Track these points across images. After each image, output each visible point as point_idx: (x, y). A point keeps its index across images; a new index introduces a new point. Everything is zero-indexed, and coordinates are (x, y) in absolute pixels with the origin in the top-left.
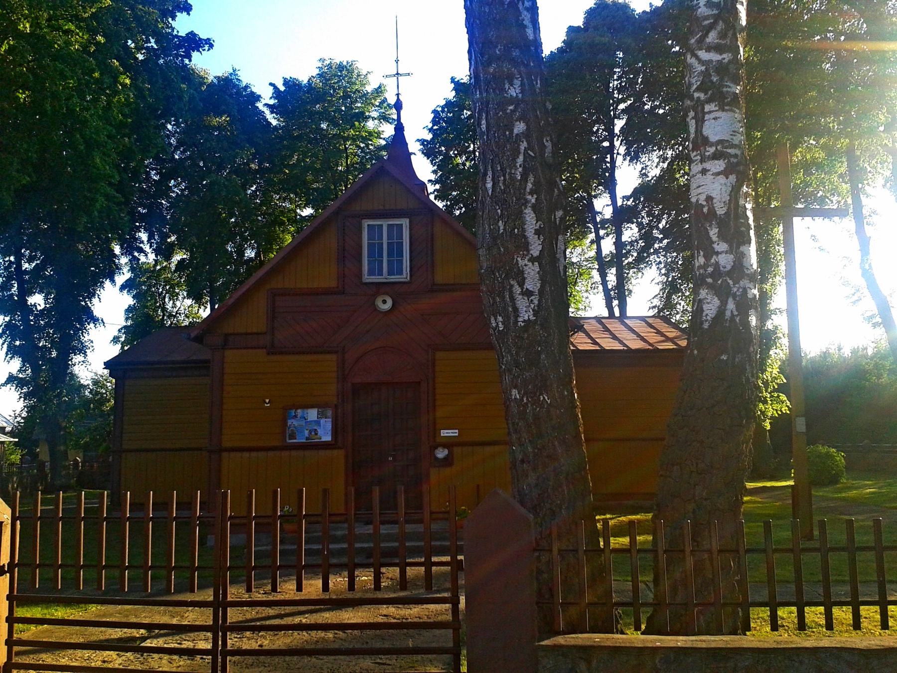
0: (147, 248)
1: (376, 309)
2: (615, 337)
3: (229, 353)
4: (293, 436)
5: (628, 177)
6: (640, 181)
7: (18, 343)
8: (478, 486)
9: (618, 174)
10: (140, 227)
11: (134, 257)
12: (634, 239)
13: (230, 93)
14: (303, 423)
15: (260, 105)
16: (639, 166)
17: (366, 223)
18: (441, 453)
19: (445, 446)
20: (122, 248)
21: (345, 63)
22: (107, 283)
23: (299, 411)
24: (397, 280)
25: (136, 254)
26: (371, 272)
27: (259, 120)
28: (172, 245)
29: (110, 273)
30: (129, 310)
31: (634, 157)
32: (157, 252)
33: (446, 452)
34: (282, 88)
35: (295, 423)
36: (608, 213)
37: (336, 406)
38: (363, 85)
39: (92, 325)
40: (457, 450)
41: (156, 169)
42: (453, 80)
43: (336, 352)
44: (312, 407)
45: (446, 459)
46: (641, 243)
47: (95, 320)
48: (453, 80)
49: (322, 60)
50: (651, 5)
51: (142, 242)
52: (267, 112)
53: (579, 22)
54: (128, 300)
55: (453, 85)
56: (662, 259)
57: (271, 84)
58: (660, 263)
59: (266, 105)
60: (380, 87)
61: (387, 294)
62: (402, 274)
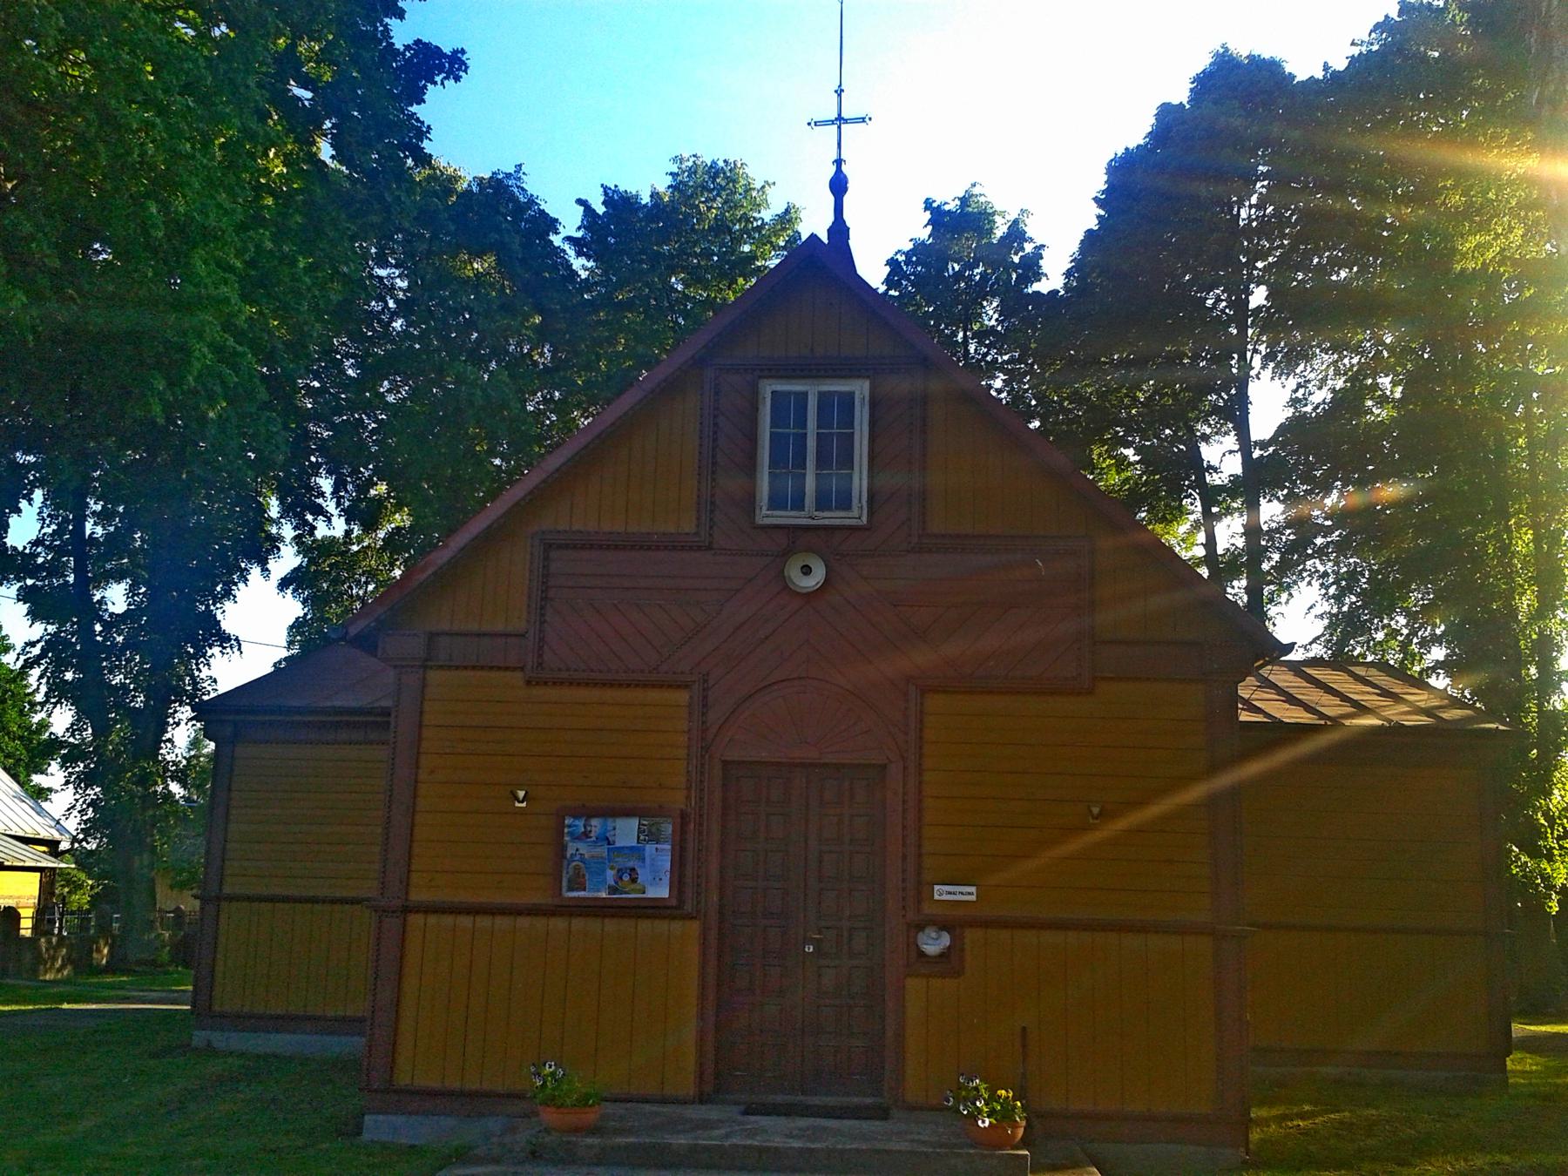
0: (331, 506)
1: (786, 588)
2: (1291, 700)
3: (434, 676)
4: (577, 883)
5: (1270, 403)
6: (1290, 412)
7: (69, 676)
8: (1024, 1029)
9: (1254, 389)
10: (318, 465)
11: (306, 522)
12: (1274, 525)
13: (502, 209)
14: (603, 851)
15: (556, 240)
16: (1292, 382)
17: (768, 388)
18: (934, 943)
19: (943, 926)
20: (282, 501)
21: (721, 164)
22: (255, 572)
23: (595, 822)
24: (837, 522)
25: (309, 517)
26: (776, 502)
27: (555, 267)
28: (379, 501)
29: (262, 549)
30: (297, 627)
31: (1286, 362)
32: (350, 515)
33: (946, 940)
34: (601, 210)
35: (584, 849)
36: (1233, 466)
37: (683, 816)
38: (757, 206)
39: (216, 650)
40: (971, 936)
41: (353, 356)
42: (928, 205)
43: (685, 686)
44: (627, 814)
45: (944, 956)
46: (1289, 535)
47: (224, 639)
48: (928, 205)
49: (679, 159)
50: (1326, 67)
51: (322, 495)
52: (571, 252)
53: (1180, 94)
54: (292, 608)
55: (928, 215)
56: (1329, 566)
57: (580, 202)
58: (1326, 574)
59: (569, 239)
60: (787, 211)
61: (809, 550)
62: (848, 507)
